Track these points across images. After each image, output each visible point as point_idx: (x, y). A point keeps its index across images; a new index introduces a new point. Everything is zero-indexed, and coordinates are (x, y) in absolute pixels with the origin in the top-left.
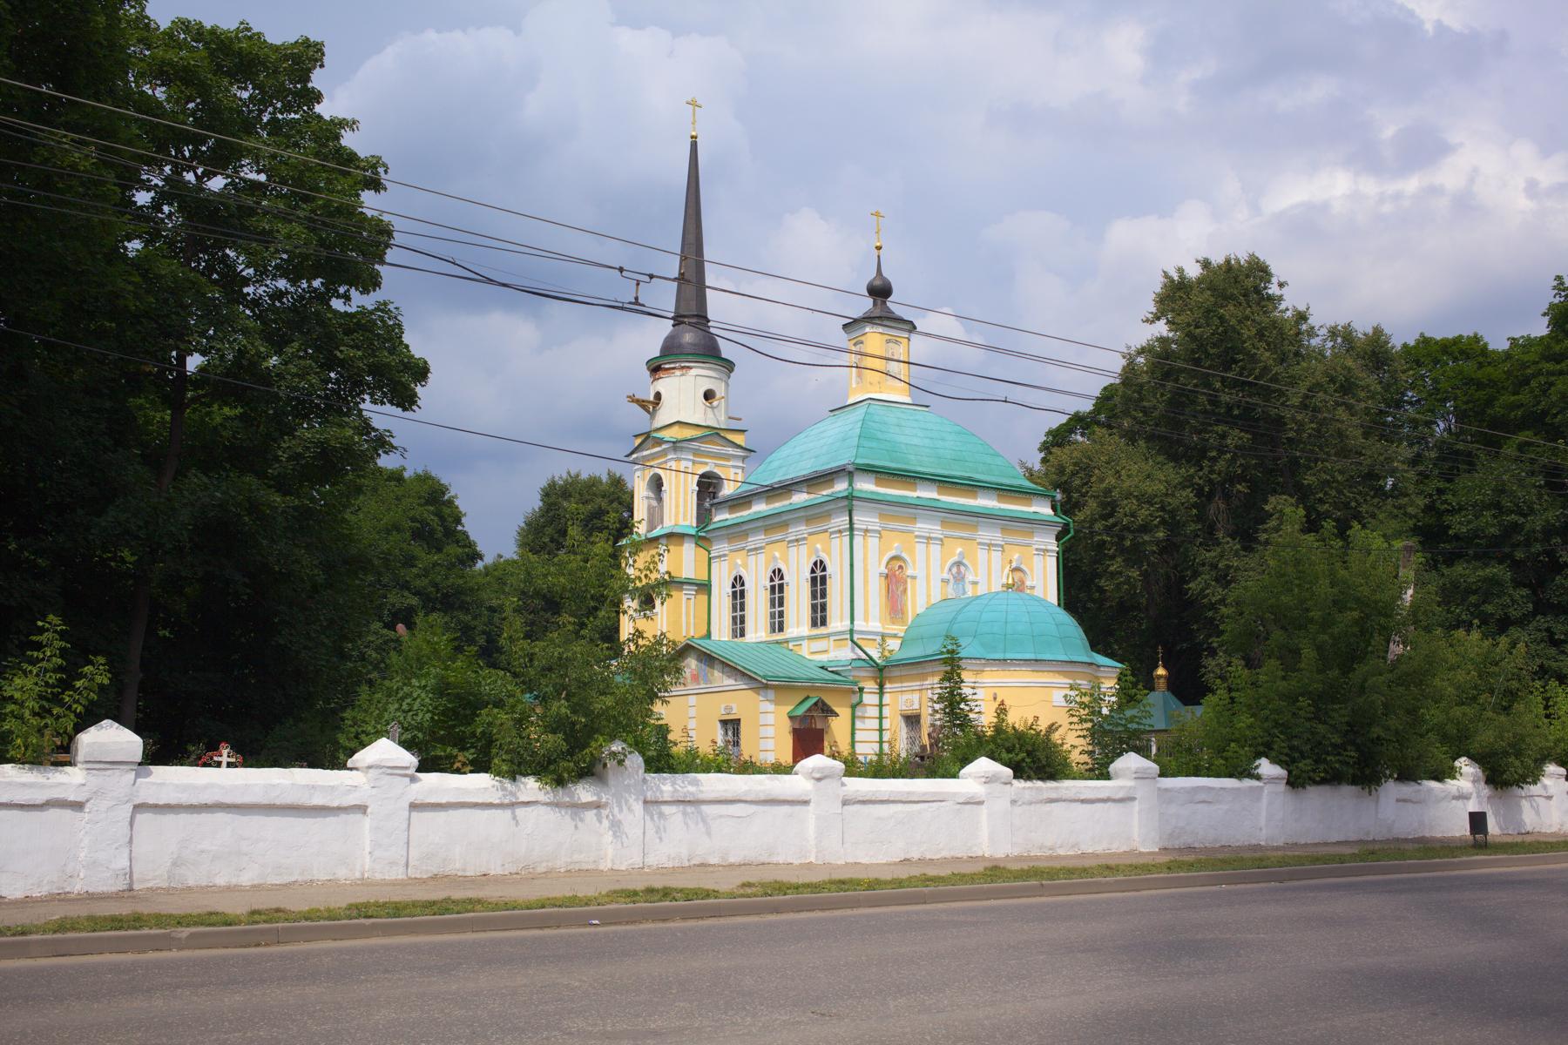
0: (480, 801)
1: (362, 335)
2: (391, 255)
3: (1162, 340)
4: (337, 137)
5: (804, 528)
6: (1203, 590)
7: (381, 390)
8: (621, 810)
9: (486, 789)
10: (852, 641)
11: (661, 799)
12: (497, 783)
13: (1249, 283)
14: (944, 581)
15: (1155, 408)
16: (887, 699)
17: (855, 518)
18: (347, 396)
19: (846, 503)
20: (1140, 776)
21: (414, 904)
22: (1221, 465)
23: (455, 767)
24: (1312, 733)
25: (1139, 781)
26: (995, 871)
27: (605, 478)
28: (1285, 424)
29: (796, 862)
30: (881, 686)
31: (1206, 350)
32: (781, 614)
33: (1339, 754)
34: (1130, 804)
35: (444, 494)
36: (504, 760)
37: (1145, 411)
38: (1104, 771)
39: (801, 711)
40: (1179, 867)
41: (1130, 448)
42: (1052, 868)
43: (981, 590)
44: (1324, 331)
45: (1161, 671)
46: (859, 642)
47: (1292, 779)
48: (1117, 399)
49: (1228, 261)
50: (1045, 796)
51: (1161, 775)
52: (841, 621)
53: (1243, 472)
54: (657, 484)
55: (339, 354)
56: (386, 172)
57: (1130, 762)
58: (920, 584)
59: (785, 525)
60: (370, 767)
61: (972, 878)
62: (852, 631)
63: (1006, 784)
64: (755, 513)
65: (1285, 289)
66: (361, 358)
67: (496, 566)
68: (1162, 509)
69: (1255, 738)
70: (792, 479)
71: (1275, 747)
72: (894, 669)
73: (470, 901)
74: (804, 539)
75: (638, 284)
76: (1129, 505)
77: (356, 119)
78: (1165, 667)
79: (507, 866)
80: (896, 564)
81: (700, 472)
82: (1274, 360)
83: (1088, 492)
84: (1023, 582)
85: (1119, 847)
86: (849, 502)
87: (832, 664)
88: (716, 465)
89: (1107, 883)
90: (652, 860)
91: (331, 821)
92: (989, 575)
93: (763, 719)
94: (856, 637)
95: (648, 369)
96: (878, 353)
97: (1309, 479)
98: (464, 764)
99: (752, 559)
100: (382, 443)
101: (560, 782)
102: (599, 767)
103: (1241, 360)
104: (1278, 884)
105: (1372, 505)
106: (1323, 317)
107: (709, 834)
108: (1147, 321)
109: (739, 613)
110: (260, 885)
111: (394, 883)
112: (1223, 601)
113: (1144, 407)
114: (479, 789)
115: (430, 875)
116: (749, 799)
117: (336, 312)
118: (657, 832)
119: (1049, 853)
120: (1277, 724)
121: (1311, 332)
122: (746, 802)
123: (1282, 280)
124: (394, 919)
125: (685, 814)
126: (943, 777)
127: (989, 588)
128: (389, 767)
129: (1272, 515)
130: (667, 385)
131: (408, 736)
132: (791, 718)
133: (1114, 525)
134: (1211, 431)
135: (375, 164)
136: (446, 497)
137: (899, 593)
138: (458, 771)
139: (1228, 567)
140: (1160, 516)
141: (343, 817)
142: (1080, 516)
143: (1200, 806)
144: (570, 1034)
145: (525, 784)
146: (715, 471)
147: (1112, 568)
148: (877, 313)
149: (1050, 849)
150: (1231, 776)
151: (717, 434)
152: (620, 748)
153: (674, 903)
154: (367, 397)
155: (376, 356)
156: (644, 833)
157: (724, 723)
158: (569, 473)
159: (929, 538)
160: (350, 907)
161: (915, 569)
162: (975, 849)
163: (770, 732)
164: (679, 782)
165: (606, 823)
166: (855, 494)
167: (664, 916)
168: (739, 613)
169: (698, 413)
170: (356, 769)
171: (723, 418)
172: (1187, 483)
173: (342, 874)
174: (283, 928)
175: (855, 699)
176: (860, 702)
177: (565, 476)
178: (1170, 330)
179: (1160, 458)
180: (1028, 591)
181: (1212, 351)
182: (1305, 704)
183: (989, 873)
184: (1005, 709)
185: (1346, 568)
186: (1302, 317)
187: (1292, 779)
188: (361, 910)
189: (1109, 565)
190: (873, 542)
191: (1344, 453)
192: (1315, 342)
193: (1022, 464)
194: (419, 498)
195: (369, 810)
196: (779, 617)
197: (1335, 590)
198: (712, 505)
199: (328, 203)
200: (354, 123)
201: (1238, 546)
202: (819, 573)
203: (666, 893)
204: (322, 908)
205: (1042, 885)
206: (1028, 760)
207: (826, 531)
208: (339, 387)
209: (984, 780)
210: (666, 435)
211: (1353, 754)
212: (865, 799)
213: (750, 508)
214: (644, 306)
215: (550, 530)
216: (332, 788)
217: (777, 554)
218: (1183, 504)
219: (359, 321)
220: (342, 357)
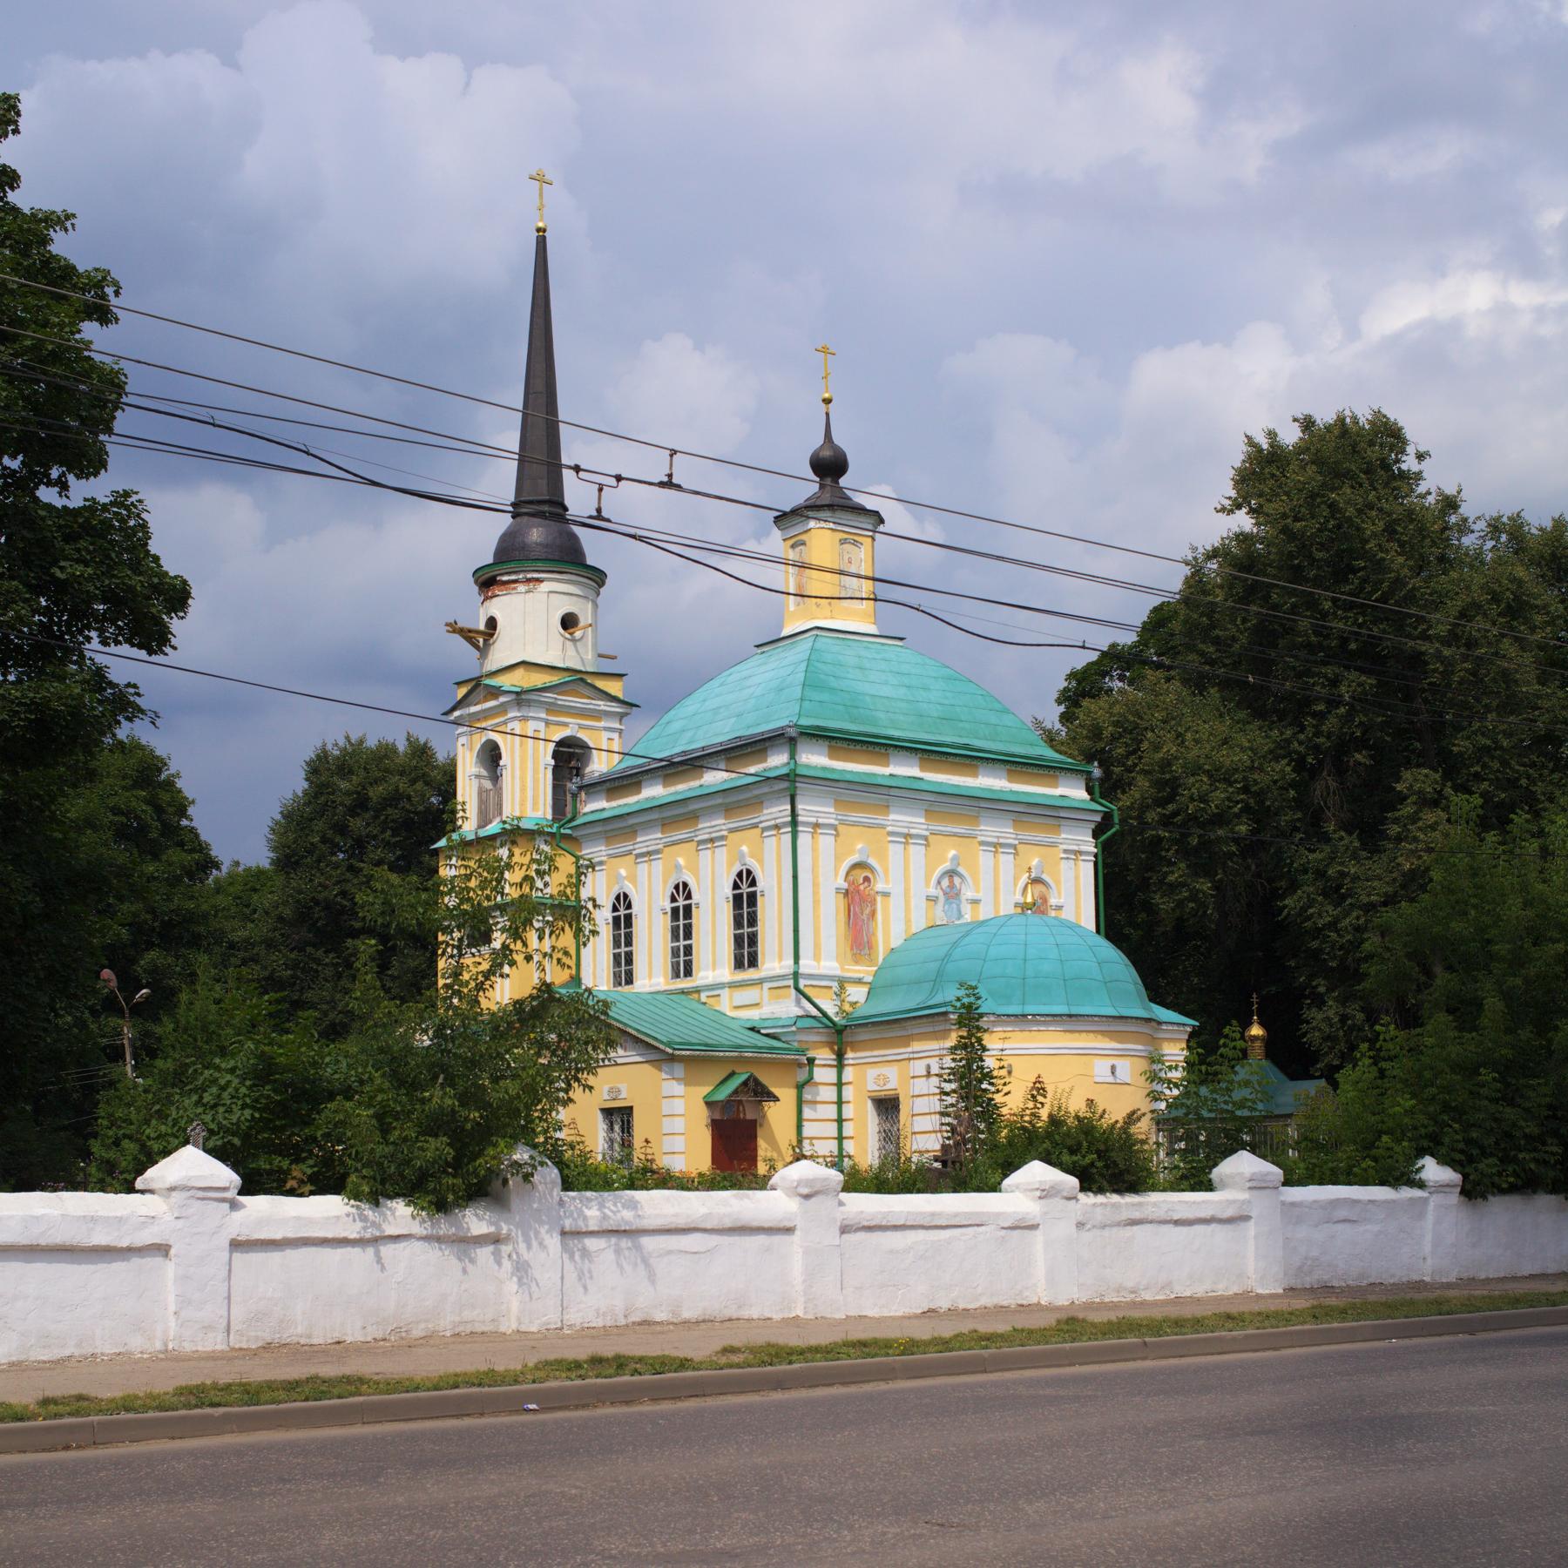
0: (330, 1235)
1: (92, 544)
2: (123, 421)
3: (1242, 538)
4: (45, 241)
5: (603, 848)
6: (1304, 909)
7: (114, 623)
8: (529, 1247)
9: (338, 1218)
10: (797, 989)
11: (584, 1230)
12: (354, 1210)
13: (1373, 453)
14: (932, 900)
15: (1234, 639)
16: (849, 1074)
17: (800, 807)
18: (63, 634)
19: (784, 785)
20: (1257, 1185)
21: (271, 1386)
22: (1331, 724)
23: (288, 1186)
24: (1496, 1120)
25: (1256, 1192)
26: (1071, 1325)
27: (402, 746)
28: (1426, 663)
29: (777, 1316)
30: (840, 1056)
31: (1311, 553)
32: (688, 950)
33: (1535, 1150)
34: (1243, 1225)
35: (160, 771)
36: (364, 1177)
37: (1217, 641)
38: (1204, 1178)
39: (723, 1094)
40: (1327, 1314)
41: (1197, 699)
42: (1152, 1320)
43: (984, 912)
44: (1481, 525)
45: (1256, 1031)
46: (808, 991)
47: (1468, 1187)
48: (1176, 626)
49: (1341, 420)
50: (1126, 1214)
51: (1286, 1183)
52: (781, 959)
53: (1363, 734)
54: (491, 756)
55: (59, 574)
56: (117, 293)
57: (1242, 1165)
58: (895, 903)
59: (692, 818)
60: (172, 1189)
61: (1041, 1335)
62: (796, 975)
63: (1069, 1199)
64: (647, 799)
65: (1428, 461)
66: (90, 579)
67: (232, 878)
68: (1246, 790)
69: (1415, 1128)
70: (703, 749)
71: (1447, 1140)
72: (860, 1030)
73: (348, 1380)
74: (723, 838)
75: (600, 490)
76: (1196, 785)
77: (70, 211)
78: (1262, 1024)
79: (369, 1329)
80: (860, 875)
81: (557, 737)
82: (1411, 569)
83: (1135, 765)
84: (1045, 900)
85: (1227, 1287)
86: (791, 784)
87: (766, 1024)
88: (581, 727)
89: (1234, 1339)
90: (576, 1317)
91: (118, 1267)
92: (996, 890)
93: (666, 1107)
94: (802, 983)
95: (476, 582)
96: (828, 564)
97: (1460, 745)
98: (302, 1182)
99: (643, 868)
100: (124, 703)
101: (441, 1206)
102: (497, 1184)
103: (1363, 568)
104: (1467, 1337)
105: (1551, 782)
106: (1478, 506)
107: (652, 1278)
108: (1223, 510)
109: (623, 949)
110: (20, 1363)
111: (213, 1357)
112: (1333, 925)
113: (1218, 637)
114: (328, 1218)
115: (260, 1344)
116: (709, 1226)
117: (49, 507)
118: (580, 1279)
119: (1130, 1297)
120: (1446, 1108)
121: (1464, 527)
122: (705, 1230)
123: (1422, 449)
124: (252, 1408)
125: (618, 1252)
126: (979, 1190)
127: (997, 911)
128: (200, 1189)
129: (1405, 798)
130: (504, 606)
131: (215, 1142)
132: (709, 1104)
133: (1175, 814)
134: (1318, 675)
135: (100, 282)
136: (163, 777)
137: (865, 917)
138: (291, 1193)
139: (1342, 874)
140: (1242, 801)
141: (136, 1262)
142: (1126, 800)
143: (1340, 1227)
144: (611, 1557)
145: (393, 1211)
146: (579, 735)
147: (1171, 878)
148: (826, 499)
149: (1132, 1292)
150: (1382, 1183)
151: (582, 680)
152: (526, 1156)
153: (636, 1378)
154: (93, 634)
155: (114, 576)
156: (562, 1278)
157: (608, 1113)
158: (347, 738)
159: (907, 836)
160: (181, 1391)
161: (887, 882)
162: (1026, 1293)
163: (679, 1125)
164: (609, 1204)
165: (507, 1265)
166: (799, 771)
167: (627, 1396)
168: (623, 949)
169: (552, 649)
170: (151, 1191)
171: (589, 656)
172: (1281, 750)
173: (137, 1344)
174: (99, 1423)
175: (802, 1075)
176: (810, 1080)
177: (342, 742)
178: (1257, 524)
179: (1242, 715)
180: (1053, 914)
181: (1319, 555)
182: (1489, 1078)
183: (1066, 1327)
184: (1043, 1089)
185: (1544, 882)
186: (1450, 504)
187: (1468, 1187)
188: (197, 1395)
189: (1166, 874)
190: (826, 841)
191: (1510, 705)
192: (1468, 541)
193: (1038, 724)
194: (124, 778)
195: (172, 1252)
196: (685, 955)
197: (1530, 913)
198: (581, 788)
199: (38, 346)
200: (68, 217)
201: (1357, 844)
202: (745, 889)
203: (620, 1363)
204: (141, 1394)
205: (1145, 1343)
206: (1099, 1164)
207: (755, 826)
208: (51, 620)
209: (1038, 1193)
210: (506, 682)
211: (1555, 1149)
212: (873, 1223)
213: (639, 792)
214: (608, 520)
215: (320, 823)
216: (120, 1219)
217: (681, 861)
218: (1275, 782)
219: (87, 520)
220: (62, 576)
